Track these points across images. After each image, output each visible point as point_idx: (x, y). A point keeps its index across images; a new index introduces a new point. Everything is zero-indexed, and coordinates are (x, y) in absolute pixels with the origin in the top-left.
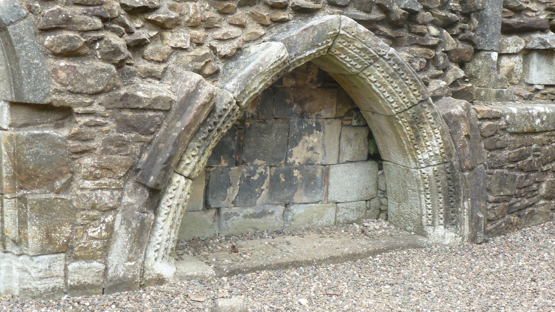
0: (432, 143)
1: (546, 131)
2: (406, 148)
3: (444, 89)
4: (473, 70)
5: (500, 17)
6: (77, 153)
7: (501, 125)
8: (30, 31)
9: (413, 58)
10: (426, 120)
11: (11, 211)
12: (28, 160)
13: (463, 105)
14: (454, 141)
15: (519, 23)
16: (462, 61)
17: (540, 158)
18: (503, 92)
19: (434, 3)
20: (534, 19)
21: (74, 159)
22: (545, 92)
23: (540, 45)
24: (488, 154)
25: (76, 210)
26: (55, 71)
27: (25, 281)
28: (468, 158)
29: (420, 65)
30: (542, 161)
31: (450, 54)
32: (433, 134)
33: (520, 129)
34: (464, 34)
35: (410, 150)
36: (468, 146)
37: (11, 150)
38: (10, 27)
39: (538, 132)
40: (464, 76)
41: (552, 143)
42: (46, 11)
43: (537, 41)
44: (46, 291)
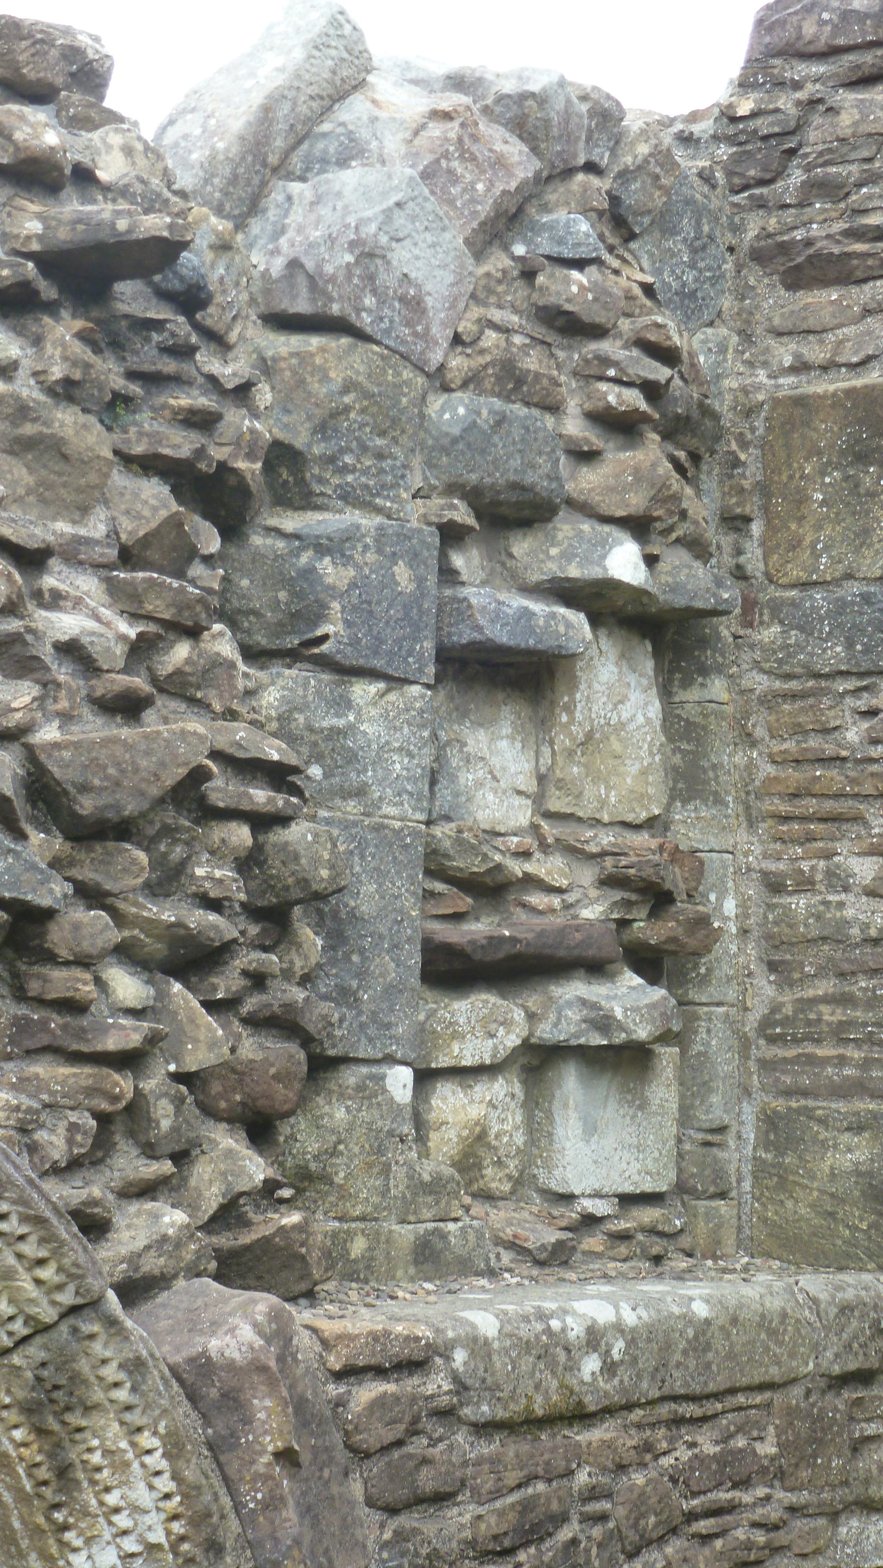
0: (132, 1495)
1: (629, 1407)
2: (17, 1525)
3: (179, 1244)
4: (313, 1147)
5: (412, 919)
7: (432, 1396)
9: (37, 1112)
10: (98, 1395)
13: (259, 1318)
14: (226, 1480)
15: (495, 941)
16: (258, 1113)
17: (611, 1525)
18: (444, 1236)
19: (125, 870)
20: (559, 920)
22: (623, 1225)
23: (587, 1030)
24: (382, 1526)
28: (296, 1553)
29: (70, 1142)
30: (621, 1539)
31: (205, 1082)
32: (130, 1455)
33: (517, 1407)
34: (264, 997)
35: (37, 1531)
36: (291, 1502)
39: (593, 1415)
40: (265, 1181)
41: (656, 1457)
43: (573, 1015)
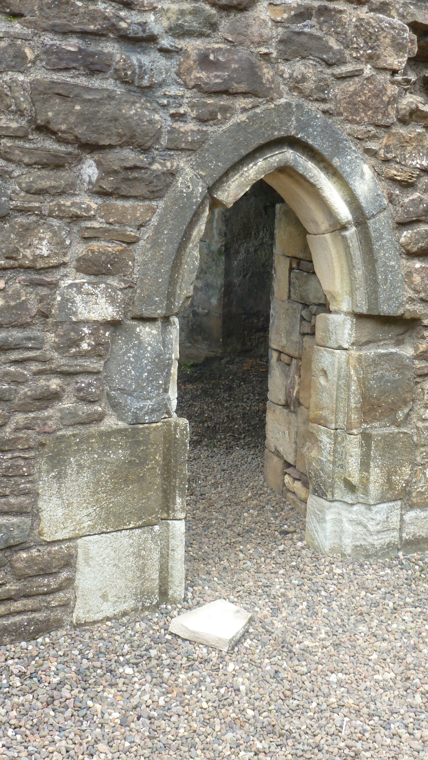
6: (420, 376)
8: (389, 226)
11: (357, 449)
12: (372, 386)
21: (417, 383)
25: (416, 446)
26: (409, 274)
27: (358, 536)
37: (360, 375)
38: (371, 221)
42: (406, 200)
44: (382, 548)
